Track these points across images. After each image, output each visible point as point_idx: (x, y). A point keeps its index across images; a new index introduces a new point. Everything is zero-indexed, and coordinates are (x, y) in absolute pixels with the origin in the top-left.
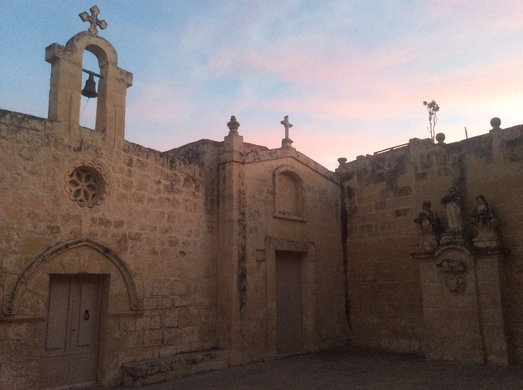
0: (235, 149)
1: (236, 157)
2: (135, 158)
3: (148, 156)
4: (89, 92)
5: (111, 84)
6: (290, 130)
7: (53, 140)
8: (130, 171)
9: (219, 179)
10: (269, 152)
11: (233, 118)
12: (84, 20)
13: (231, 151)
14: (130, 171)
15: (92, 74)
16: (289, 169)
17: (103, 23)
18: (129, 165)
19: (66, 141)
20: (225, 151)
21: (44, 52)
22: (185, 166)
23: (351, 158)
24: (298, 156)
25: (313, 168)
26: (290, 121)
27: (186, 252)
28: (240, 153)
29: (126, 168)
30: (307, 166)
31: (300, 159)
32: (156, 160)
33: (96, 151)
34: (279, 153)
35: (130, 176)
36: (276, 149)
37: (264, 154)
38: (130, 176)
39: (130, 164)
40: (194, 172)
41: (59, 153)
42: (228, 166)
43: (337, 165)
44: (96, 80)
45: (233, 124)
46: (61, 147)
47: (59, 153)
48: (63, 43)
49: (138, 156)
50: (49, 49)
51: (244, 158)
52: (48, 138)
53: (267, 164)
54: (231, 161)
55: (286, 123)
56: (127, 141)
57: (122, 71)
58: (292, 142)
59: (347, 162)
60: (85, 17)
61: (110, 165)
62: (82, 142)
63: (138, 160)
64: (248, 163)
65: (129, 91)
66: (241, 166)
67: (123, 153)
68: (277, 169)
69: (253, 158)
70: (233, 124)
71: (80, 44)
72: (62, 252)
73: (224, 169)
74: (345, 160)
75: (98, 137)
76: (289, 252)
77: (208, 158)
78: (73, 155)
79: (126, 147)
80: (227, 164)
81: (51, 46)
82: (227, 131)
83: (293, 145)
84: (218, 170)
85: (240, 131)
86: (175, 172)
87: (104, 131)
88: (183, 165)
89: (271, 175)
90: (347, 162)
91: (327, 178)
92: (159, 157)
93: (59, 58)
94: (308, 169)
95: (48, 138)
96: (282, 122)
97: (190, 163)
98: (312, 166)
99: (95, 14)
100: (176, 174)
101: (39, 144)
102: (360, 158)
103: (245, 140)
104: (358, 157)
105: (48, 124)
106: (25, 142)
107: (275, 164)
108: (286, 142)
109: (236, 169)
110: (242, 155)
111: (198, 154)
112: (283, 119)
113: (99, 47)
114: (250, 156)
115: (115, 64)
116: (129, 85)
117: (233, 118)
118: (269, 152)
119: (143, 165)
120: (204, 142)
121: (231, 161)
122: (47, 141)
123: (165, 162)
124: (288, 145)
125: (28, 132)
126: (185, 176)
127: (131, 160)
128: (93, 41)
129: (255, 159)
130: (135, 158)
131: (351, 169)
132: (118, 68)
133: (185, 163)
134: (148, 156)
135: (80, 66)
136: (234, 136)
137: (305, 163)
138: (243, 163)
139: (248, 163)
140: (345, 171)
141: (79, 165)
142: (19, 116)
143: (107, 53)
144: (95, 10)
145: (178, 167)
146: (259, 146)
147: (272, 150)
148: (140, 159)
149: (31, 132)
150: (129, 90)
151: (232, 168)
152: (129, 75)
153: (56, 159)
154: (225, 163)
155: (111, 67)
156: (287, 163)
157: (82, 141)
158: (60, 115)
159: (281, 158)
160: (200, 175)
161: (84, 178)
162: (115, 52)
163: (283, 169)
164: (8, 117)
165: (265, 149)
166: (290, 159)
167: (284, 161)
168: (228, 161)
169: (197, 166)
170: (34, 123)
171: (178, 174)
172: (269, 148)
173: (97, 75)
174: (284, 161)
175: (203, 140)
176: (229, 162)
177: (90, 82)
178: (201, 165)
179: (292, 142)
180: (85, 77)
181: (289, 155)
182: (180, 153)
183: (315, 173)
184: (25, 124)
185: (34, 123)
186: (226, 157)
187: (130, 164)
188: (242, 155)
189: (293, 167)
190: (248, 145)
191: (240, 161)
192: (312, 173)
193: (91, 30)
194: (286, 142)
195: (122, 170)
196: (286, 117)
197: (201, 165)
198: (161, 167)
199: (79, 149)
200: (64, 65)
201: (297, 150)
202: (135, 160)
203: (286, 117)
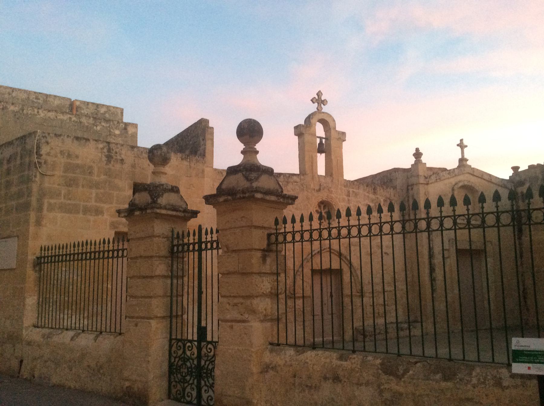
0: (420, 174)
1: (422, 180)
2: (351, 190)
3: (359, 188)
4: (320, 151)
5: (333, 143)
6: (465, 150)
7: (305, 186)
8: (349, 200)
9: (408, 197)
10: (448, 172)
11: (417, 150)
12: (314, 103)
13: (418, 176)
14: (349, 200)
15: (321, 138)
16: (466, 183)
17: (325, 101)
18: (347, 196)
19: (312, 186)
20: (411, 176)
21: (293, 130)
22: (384, 191)
23: (523, 167)
24: (474, 172)
25: (488, 179)
26: (465, 143)
27: (388, 253)
28: (425, 176)
29: (346, 198)
30: (481, 178)
31: (475, 174)
32: (364, 190)
33: (328, 190)
34: (456, 171)
35: (349, 203)
36: (454, 169)
37: (444, 175)
38: (349, 203)
39: (348, 195)
40: (390, 194)
41: (309, 194)
42: (415, 188)
43: (511, 173)
44: (324, 141)
45: (418, 154)
46: (309, 191)
47: (309, 194)
48: (303, 123)
49: (353, 188)
50: (296, 128)
51: (427, 180)
52: (303, 186)
53: (446, 181)
54: (418, 184)
55: (462, 145)
56: (346, 180)
57: (339, 133)
58: (467, 160)
59: (520, 170)
60: (314, 100)
61: (337, 198)
62: (320, 185)
63: (353, 192)
64: (431, 183)
65: (344, 143)
66: (426, 186)
67: (344, 188)
68: (456, 184)
69: (435, 178)
70: (418, 154)
71: (313, 121)
72: (521, 258)
73: (412, 189)
74: (518, 168)
75: (329, 179)
76: (58, 386)
77: (399, 182)
78: (316, 194)
79: (345, 184)
80: (415, 186)
81: (298, 126)
82: (413, 160)
83: (468, 163)
84: (408, 190)
85: (424, 159)
86: (377, 196)
87: (331, 175)
88: (382, 190)
89: (450, 190)
90: (520, 170)
91: (501, 186)
92: (365, 187)
93: (303, 134)
94: (484, 181)
95: (303, 186)
96: (458, 145)
97: (387, 188)
98: (486, 177)
99: (320, 97)
100: (377, 198)
101: (299, 191)
102: (531, 167)
103: (428, 166)
104: (529, 166)
105: (302, 177)
106: (291, 191)
107: (453, 181)
108: (463, 161)
109: (422, 189)
110: (426, 178)
111: (392, 180)
112: (459, 142)
113: (324, 119)
114: (432, 177)
115: (335, 128)
116: (344, 140)
117: (417, 150)
118: (448, 172)
119: (356, 195)
120: (396, 170)
121: (418, 184)
122: (302, 188)
123: (370, 190)
124: (464, 163)
125: (292, 184)
126: (384, 198)
127: (349, 192)
128: (321, 116)
129: (437, 180)
130: (351, 190)
131: (523, 177)
132: (337, 131)
133: (383, 189)
134: (359, 188)
135: (315, 135)
136: (419, 164)
137: (480, 176)
138: (427, 184)
139: (431, 183)
140: (518, 179)
141: (321, 200)
142: (287, 175)
143: (329, 121)
144: (320, 94)
145: (378, 192)
146: (439, 168)
147: (450, 170)
148: (354, 190)
149: (294, 184)
150: (344, 143)
151: (418, 189)
152: (344, 134)
153: (308, 198)
154: (413, 185)
155: (333, 131)
156: (464, 179)
157: (320, 185)
158: (308, 171)
159: (459, 175)
160: (394, 196)
161: (322, 208)
162: (334, 121)
163: (461, 184)
164: (282, 176)
165: (445, 170)
166: (467, 175)
167: (461, 178)
168: (415, 183)
169: (392, 189)
170: (295, 178)
171: (379, 197)
172: (448, 169)
173: (324, 138)
174: (461, 178)
175: (394, 168)
176: (416, 184)
177: (321, 143)
178: (395, 188)
179: (467, 160)
180: (318, 141)
181: (465, 172)
182: (377, 179)
183: (490, 183)
184: (290, 180)
185: (295, 178)
186: (413, 180)
187: (348, 195)
188: (426, 178)
189: (469, 181)
190: (431, 169)
191: (425, 183)
192: (486, 183)
193: (319, 108)
194: (463, 161)
195: (344, 200)
196: (462, 140)
197: (395, 188)
198: (367, 194)
199: (319, 190)
200: (307, 137)
201: (472, 167)
202: (351, 192)
203: (462, 140)
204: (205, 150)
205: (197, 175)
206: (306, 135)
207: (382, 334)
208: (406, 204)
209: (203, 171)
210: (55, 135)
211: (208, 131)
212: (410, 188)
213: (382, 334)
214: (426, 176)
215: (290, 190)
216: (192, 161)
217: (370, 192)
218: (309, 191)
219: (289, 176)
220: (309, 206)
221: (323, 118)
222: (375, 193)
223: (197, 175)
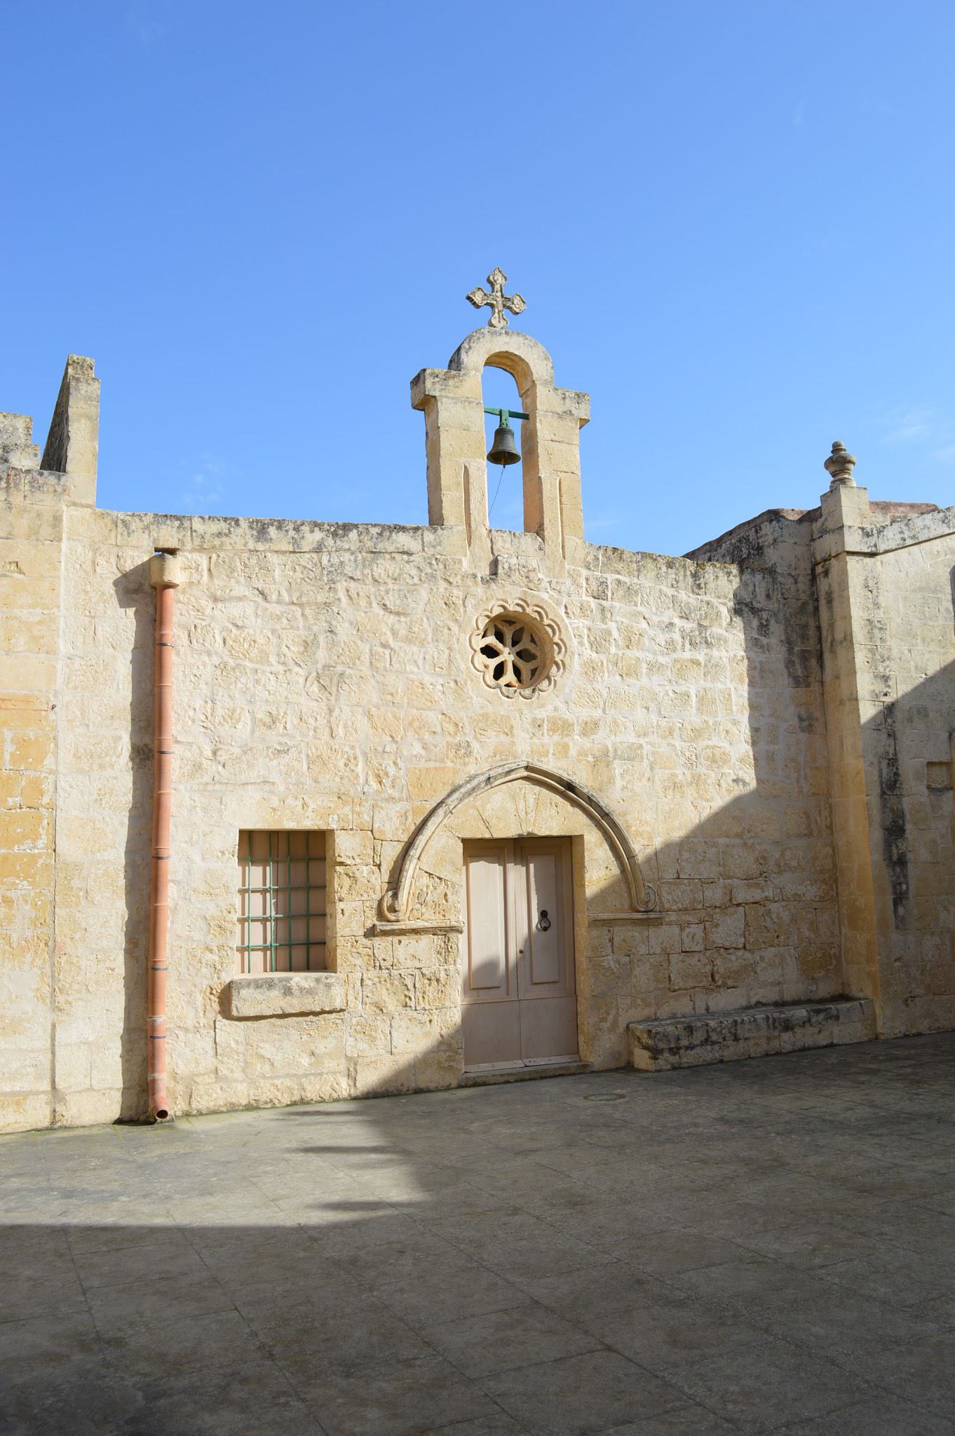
2: (611, 578)
9: (817, 600)
11: (836, 448)
19: (466, 565)
47: (455, 591)
49: (619, 573)
51: (872, 541)
67: (585, 572)
73: (826, 573)
78: (480, 590)
84: (813, 578)
86: (706, 598)
92: (664, 569)
101: (416, 580)
105: (429, 537)
117: (836, 448)
122: (429, 571)
127: (603, 583)
130: (611, 578)
141: (497, 611)
145: (711, 585)
160: (768, 596)
198: (670, 592)
204: (829, 795)
205: (33, 533)
206: (444, 400)
207: (714, 1043)
208: (869, 647)
209: (57, 520)
210: (217, 750)
211: (77, 389)
212: (819, 569)
213: (714, 1043)
214: (868, 527)
215: (384, 576)
216: (16, 485)
217: (681, 584)
218: (456, 580)
219: (380, 534)
220: (455, 628)
221: (504, 349)
222: (699, 586)
223: (33, 533)
